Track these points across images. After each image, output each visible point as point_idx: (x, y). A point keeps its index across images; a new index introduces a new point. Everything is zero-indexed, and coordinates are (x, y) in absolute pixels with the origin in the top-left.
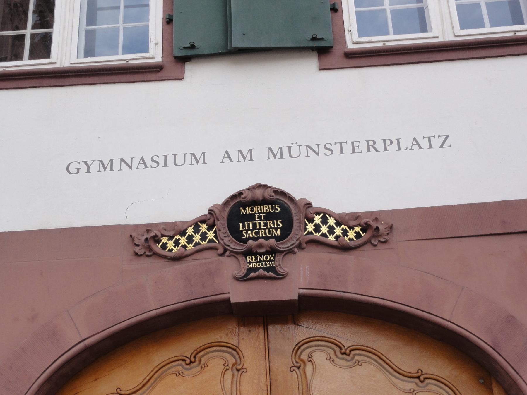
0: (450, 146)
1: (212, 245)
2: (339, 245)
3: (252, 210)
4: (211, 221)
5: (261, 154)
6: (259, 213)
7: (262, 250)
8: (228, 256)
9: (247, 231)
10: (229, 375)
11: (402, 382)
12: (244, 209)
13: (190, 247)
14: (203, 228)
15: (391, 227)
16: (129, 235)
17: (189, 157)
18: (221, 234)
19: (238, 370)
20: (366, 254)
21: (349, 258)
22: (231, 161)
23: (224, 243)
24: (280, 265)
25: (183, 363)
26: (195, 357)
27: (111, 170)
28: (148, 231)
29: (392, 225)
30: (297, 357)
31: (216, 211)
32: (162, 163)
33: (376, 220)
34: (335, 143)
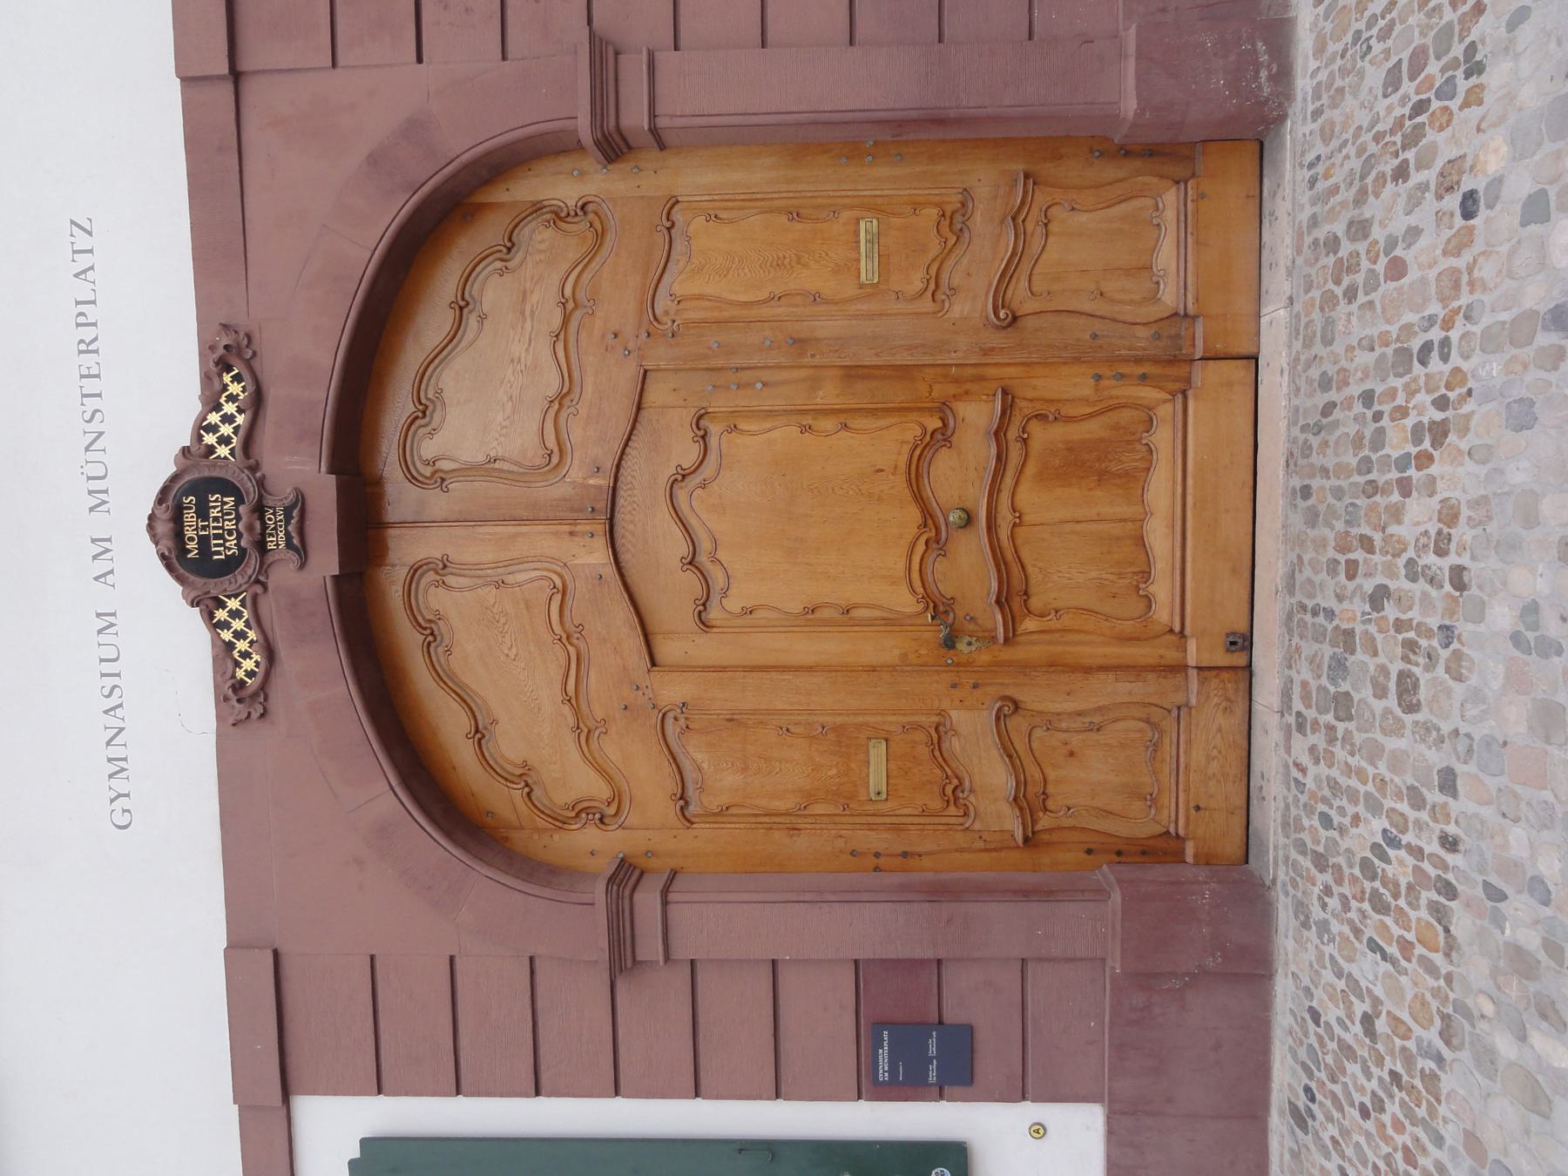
0: (90, 220)
1: (249, 602)
2: (253, 409)
3: (191, 539)
4: (211, 603)
5: (99, 524)
6: (196, 529)
7: (258, 525)
8: (267, 578)
9: (226, 548)
10: (450, 580)
11: (468, 331)
12: (190, 551)
13: (252, 635)
14: (221, 615)
15: (225, 327)
16: (233, 728)
17: (103, 638)
18: (231, 589)
19: (445, 566)
20: (272, 367)
21: (273, 394)
22: (111, 572)
23: (246, 583)
24: (282, 500)
25: (433, 645)
26: (425, 629)
27: (125, 759)
28: (226, 699)
29: (221, 324)
30: (427, 481)
31: (193, 595)
32: (115, 680)
33: (212, 348)
34: (82, 404)
